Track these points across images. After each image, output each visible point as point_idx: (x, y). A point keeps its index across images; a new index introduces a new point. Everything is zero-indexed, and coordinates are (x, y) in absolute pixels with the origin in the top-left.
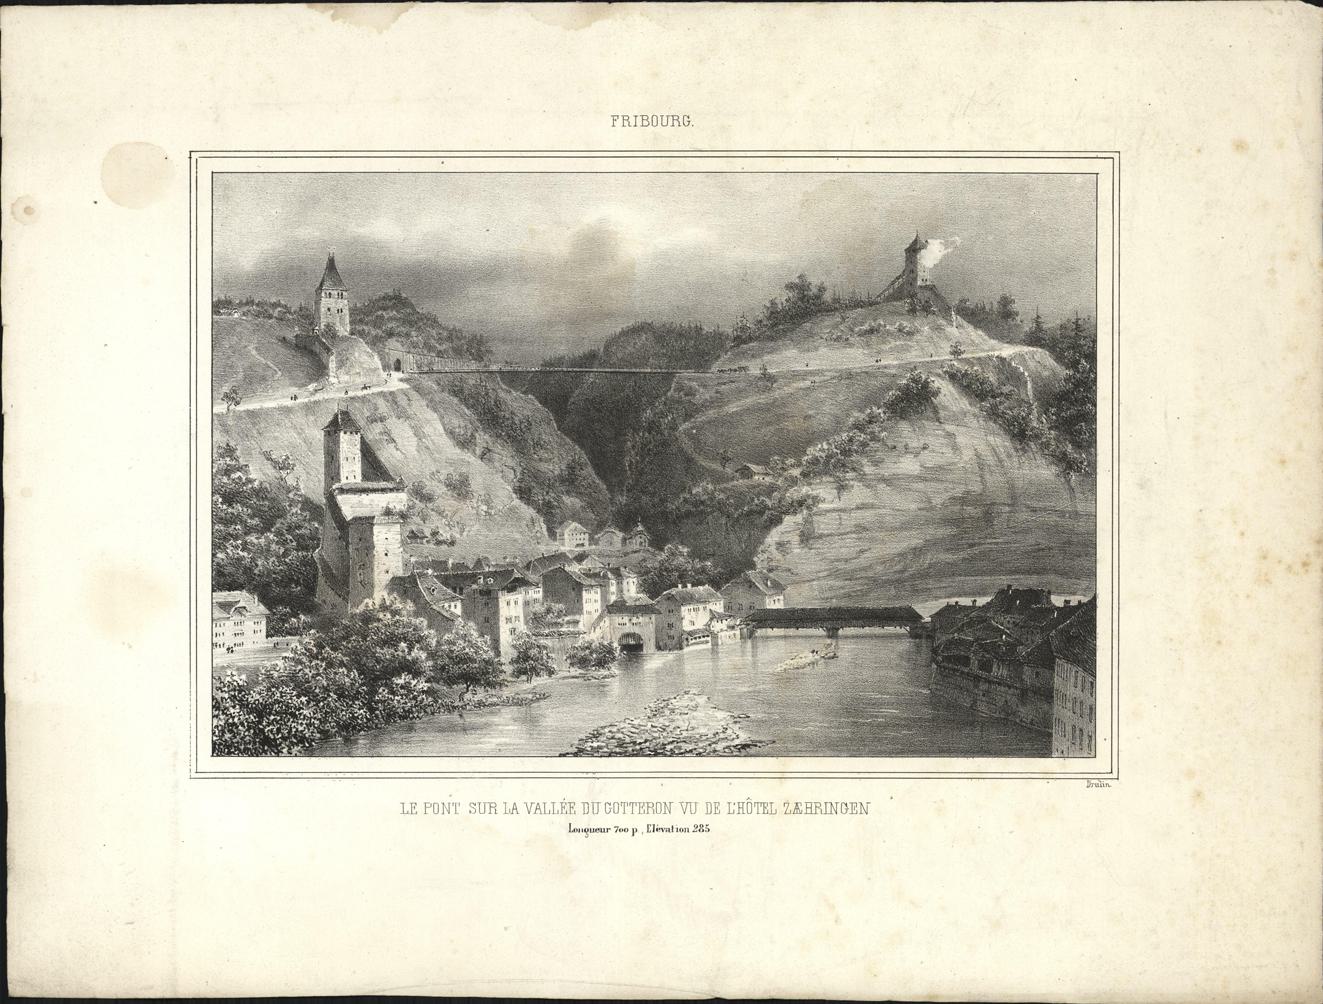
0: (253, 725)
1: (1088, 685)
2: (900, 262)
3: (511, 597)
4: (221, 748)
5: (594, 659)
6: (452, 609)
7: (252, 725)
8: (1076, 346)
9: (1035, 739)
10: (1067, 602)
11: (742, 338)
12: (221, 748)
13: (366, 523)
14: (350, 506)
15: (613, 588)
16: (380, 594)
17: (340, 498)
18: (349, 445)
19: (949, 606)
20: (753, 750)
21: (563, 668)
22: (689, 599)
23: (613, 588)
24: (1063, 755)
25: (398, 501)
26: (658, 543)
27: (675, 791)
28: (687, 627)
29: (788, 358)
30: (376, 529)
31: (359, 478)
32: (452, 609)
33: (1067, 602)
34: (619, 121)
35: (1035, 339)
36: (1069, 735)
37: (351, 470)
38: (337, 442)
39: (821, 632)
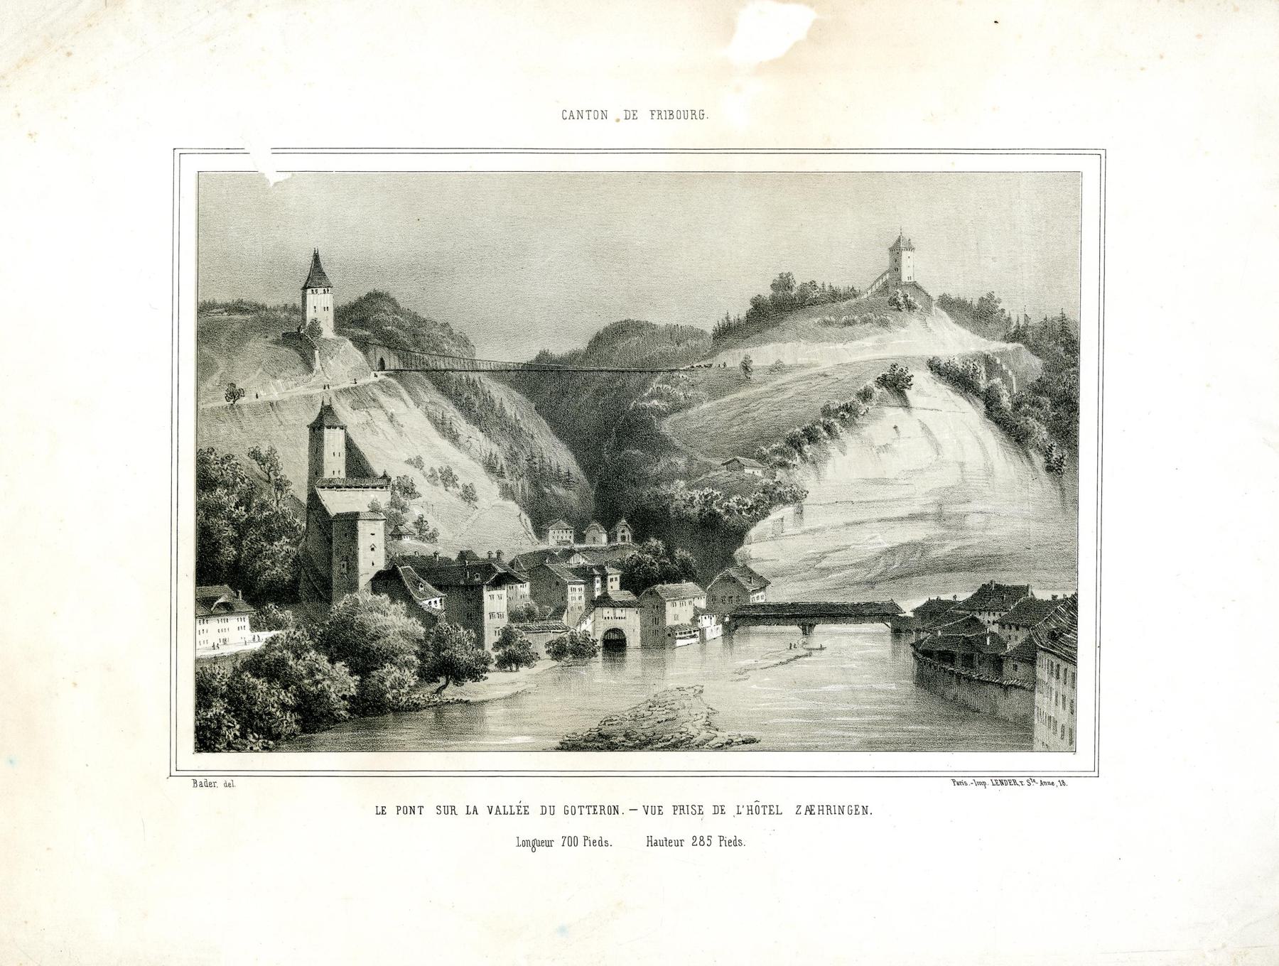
0: (233, 714)
1: (1069, 680)
2: (886, 262)
3: (495, 593)
4: (207, 739)
5: (571, 651)
6: (433, 605)
7: (233, 714)
8: (1060, 343)
9: (1020, 733)
10: (1054, 597)
11: (727, 333)
12: (207, 739)
13: (350, 521)
14: (336, 502)
15: (598, 585)
16: (364, 595)
17: (320, 491)
18: (333, 441)
19: (930, 603)
20: (752, 746)
21: (545, 663)
22: (677, 596)
23: (598, 585)
24: (1047, 748)
25: (383, 498)
26: (639, 537)
27: (704, 793)
28: (670, 621)
29: (763, 354)
30: (360, 524)
31: (343, 475)
32: (433, 605)
33: (1054, 597)
34: (656, 114)
35: (1018, 336)
36: (1059, 734)
37: (335, 465)
38: (321, 439)
39: (795, 628)
